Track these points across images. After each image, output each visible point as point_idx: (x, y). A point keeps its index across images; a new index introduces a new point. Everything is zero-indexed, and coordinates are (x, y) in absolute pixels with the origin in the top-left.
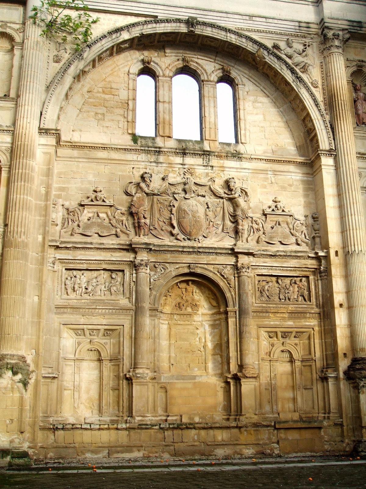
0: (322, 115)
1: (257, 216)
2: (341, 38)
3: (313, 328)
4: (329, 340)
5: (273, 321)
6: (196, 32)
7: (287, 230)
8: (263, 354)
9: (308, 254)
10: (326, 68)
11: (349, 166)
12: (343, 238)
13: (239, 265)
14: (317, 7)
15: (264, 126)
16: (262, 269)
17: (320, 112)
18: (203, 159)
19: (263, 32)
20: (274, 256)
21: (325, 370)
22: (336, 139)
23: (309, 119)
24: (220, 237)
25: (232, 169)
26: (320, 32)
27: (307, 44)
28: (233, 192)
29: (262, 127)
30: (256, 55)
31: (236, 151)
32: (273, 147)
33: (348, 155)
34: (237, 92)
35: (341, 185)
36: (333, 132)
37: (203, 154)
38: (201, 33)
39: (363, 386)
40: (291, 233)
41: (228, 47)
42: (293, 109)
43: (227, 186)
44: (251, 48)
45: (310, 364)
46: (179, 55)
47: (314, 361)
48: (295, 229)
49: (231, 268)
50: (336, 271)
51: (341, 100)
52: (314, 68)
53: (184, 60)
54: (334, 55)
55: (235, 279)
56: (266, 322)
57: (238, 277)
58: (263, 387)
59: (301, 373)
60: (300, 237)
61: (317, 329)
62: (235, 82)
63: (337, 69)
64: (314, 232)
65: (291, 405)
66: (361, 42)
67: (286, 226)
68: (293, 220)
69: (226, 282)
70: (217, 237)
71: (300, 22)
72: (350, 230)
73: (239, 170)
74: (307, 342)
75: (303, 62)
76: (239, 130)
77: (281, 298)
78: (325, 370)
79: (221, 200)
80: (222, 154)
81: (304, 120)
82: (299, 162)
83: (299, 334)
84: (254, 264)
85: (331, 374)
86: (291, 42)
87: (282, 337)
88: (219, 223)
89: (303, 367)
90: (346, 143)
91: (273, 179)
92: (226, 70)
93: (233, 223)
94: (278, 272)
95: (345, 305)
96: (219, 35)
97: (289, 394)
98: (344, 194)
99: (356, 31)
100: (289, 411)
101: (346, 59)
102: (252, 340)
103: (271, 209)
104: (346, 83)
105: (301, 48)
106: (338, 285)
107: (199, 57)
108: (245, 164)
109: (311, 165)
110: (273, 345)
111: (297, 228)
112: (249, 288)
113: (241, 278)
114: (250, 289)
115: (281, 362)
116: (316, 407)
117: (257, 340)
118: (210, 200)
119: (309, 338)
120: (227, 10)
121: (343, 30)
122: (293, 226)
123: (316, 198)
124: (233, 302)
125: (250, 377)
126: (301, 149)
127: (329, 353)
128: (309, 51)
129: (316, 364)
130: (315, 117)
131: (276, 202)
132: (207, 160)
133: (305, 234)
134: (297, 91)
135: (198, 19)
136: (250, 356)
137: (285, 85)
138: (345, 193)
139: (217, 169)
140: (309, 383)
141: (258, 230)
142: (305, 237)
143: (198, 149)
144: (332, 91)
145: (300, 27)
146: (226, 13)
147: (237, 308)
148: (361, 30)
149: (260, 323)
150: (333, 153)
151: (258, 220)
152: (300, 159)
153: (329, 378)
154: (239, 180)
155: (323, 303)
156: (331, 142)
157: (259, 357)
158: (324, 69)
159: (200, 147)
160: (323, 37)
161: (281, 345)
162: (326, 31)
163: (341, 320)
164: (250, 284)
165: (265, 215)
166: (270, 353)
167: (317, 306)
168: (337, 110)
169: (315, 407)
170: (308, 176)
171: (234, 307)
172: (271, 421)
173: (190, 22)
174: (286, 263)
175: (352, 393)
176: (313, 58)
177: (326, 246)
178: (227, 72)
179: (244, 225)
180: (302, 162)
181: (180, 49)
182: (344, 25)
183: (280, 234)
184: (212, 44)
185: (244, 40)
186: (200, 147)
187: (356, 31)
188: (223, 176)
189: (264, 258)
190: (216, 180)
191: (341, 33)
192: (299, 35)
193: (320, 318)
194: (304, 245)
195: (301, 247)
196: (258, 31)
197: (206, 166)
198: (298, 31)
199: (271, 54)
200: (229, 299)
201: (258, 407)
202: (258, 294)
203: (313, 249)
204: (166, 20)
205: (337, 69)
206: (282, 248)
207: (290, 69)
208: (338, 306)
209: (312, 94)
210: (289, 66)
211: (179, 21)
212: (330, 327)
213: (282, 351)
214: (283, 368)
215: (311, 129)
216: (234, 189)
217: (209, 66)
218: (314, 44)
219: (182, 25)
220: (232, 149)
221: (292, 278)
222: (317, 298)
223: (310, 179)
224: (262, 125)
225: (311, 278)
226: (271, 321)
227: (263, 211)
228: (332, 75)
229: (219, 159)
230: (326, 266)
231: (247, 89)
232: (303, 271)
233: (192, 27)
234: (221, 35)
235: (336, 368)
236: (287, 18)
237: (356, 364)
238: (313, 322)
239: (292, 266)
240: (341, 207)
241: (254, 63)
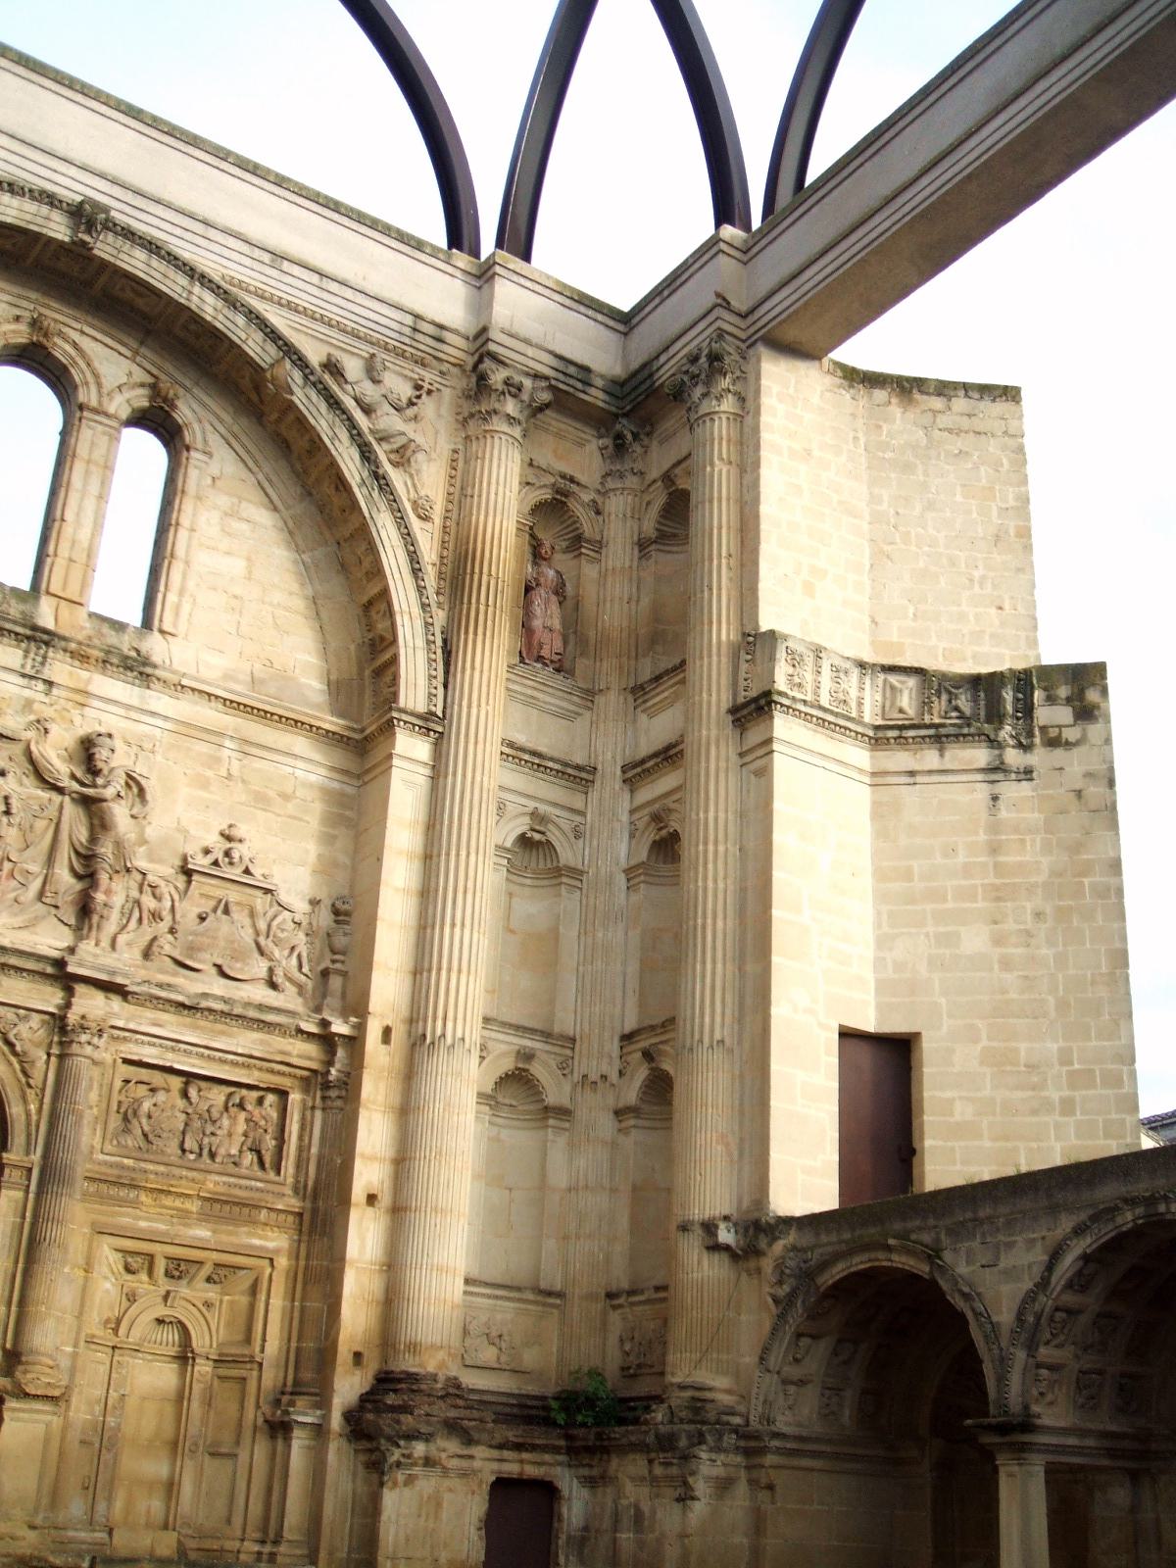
0: (424, 607)
1: (162, 871)
2: (525, 397)
3: (271, 1260)
4: (314, 1304)
5: (146, 1218)
6: (96, 252)
7: (247, 935)
8: (94, 1325)
9: (297, 1021)
10: (466, 472)
11: (473, 777)
12: (413, 993)
13: (72, 1017)
14: (475, 290)
15: (242, 596)
16: (143, 1043)
17: (421, 595)
18: (27, 652)
19: (305, 312)
20: (190, 1008)
21: (285, 1399)
22: (450, 687)
23: (383, 607)
24: (26, 917)
25: (111, 706)
26: (471, 361)
27: (426, 386)
28: (100, 781)
29: (235, 597)
30: (268, 375)
31: (138, 651)
32: (258, 666)
33: (476, 743)
34: (182, 471)
35: (438, 827)
36: (447, 664)
37: (28, 638)
38: (112, 260)
39: (398, 1464)
40: (258, 945)
41: (185, 327)
42: (344, 568)
43: (83, 755)
44: (258, 350)
45: (243, 1373)
46: (25, 304)
47: (256, 1366)
48: (272, 933)
49: (43, 1022)
50: (376, 1090)
51: (490, 575)
52: (430, 460)
53: (35, 324)
54: (496, 440)
55: (48, 1062)
56: (125, 1219)
57: (62, 1057)
58: (74, 1436)
59: (208, 1402)
60: (284, 962)
61: (282, 1262)
62: (182, 438)
63: (498, 483)
64: (329, 956)
65: (157, 1505)
66: (578, 426)
67: (247, 922)
68: (271, 906)
69: (17, 1066)
70: (16, 915)
71: (417, 316)
72: (439, 969)
73: (134, 715)
74: (244, 1300)
75: (404, 434)
76: (162, 588)
77: (187, 1146)
78: (285, 1399)
79: (57, 798)
80: (90, 651)
81: (368, 606)
82: (328, 731)
83: (222, 1272)
84: (121, 1024)
85: (305, 1414)
86: (379, 366)
87: (168, 1274)
88: (35, 868)
89: (216, 1382)
90: (479, 706)
91: (236, 764)
92: (163, 393)
93: (79, 877)
94: (191, 1061)
95: (385, 1200)
96: (167, 282)
97: (158, 1468)
98: (443, 857)
99: (571, 390)
100: (148, 1525)
101: (528, 460)
102: (66, 1270)
103: (210, 859)
104: (514, 530)
105: (405, 391)
106: (374, 1133)
107: (87, 329)
108: (159, 701)
109: (361, 749)
110: (132, 1298)
111: (281, 935)
112: (90, 1097)
113: (68, 1062)
114: (94, 1104)
115: (150, 1357)
116: (238, 1520)
117: (82, 1273)
118: (19, 789)
119: (254, 1290)
120: (211, 216)
121: (536, 376)
122: (269, 926)
123: (356, 851)
124: (29, 1135)
125: (36, 1397)
126: (340, 692)
127: (310, 1345)
128: (427, 407)
129: (260, 1377)
130: (405, 607)
131: (229, 838)
132: (39, 659)
133: (299, 957)
134: (367, 515)
135: (113, 213)
136: (50, 1323)
137: (333, 486)
138: (448, 854)
139: (63, 693)
140: (227, 1437)
141: (156, 916)
142: (300, 967)
143: (18, 615)
144: (468, 543)
145: (415, 329)
146: (206, 223)
147: (36, 1157)
148: (584, 392)
149: (103, 1219)
150: (435, 726)
151: (162, 883)
152: (332, 723)
153: (295, 1426)
154: (129, 744)
155: (317, 1181)
156: (434, 691)
157: (78, 1333)
158: (459, 473)
159: (23, 613)
160: (474, 379)
161: (160, 1300)
162: (487, 364)
163: (363, 1246)
164: (96, 1086)
165: (188, 873)
166: (119, 1322)
167: (296, 1190)
168: (474, 600)
169: (233, 1519)
170: (345, 779)
171: (28, 1153)
172: (80, 1555)
173: (85, 215)
174: (224, 1038)
175: (359, 1482)
176: (432, 431)
177: (357, 1007)
178: (165, 400)
179: (114, 893)
180: (334, 733)
181: (31, 289)
182: (543, 364)
183: (222, 944)
184: (140, 303)
185: (241, 320)
186: (23, 613)
187: (571, 390)
188: (78, 720)
189: (155, 1008)
190: (54, 728)
191: (528, 383)
192: (408, 354)
193: (301, 1231)
194: (291, 989)
195: (281, 996)
196: (291, 307)
197: (32, 677)
198: (407, 341)
199: (314, 384)
200: (16, 1125)
201: (45, 1501)
202: (115, 1121)
203: (318, 1009)
204: (10, 184)
205: (498, 483)
206: (219, 987)
207: (359, 446)
208: (363, 1199)
209: (409, 534)
210: (359, 434)
211: (50, 199)
212: (325, 1263)
213: (160, 1321)
214: (154, 1376)
215: (382, 639)
216: (105, 772)
217: (113, 368)
218: (447, 392)
219: (58, 217)
220: (125, 643)
221: (233, 1089)
222: (301, 1163)
223: (349, 790)
224: (238, 591)
225: (295, 1097)
226: (140, 1218)
227: (185, 859)
228: (480, 496)
229: (77, 663)
230: (348, 1069)
231: (214, 468)
232: (272, 1071)
233: (89, 232)
234: (174, 285)
235: (322, 1399)
236: (385, 294)
237: (387, 1391)
238: (276, 1241)
239: (240, 1051)
240: (427, 894)
241: (254, 397)
